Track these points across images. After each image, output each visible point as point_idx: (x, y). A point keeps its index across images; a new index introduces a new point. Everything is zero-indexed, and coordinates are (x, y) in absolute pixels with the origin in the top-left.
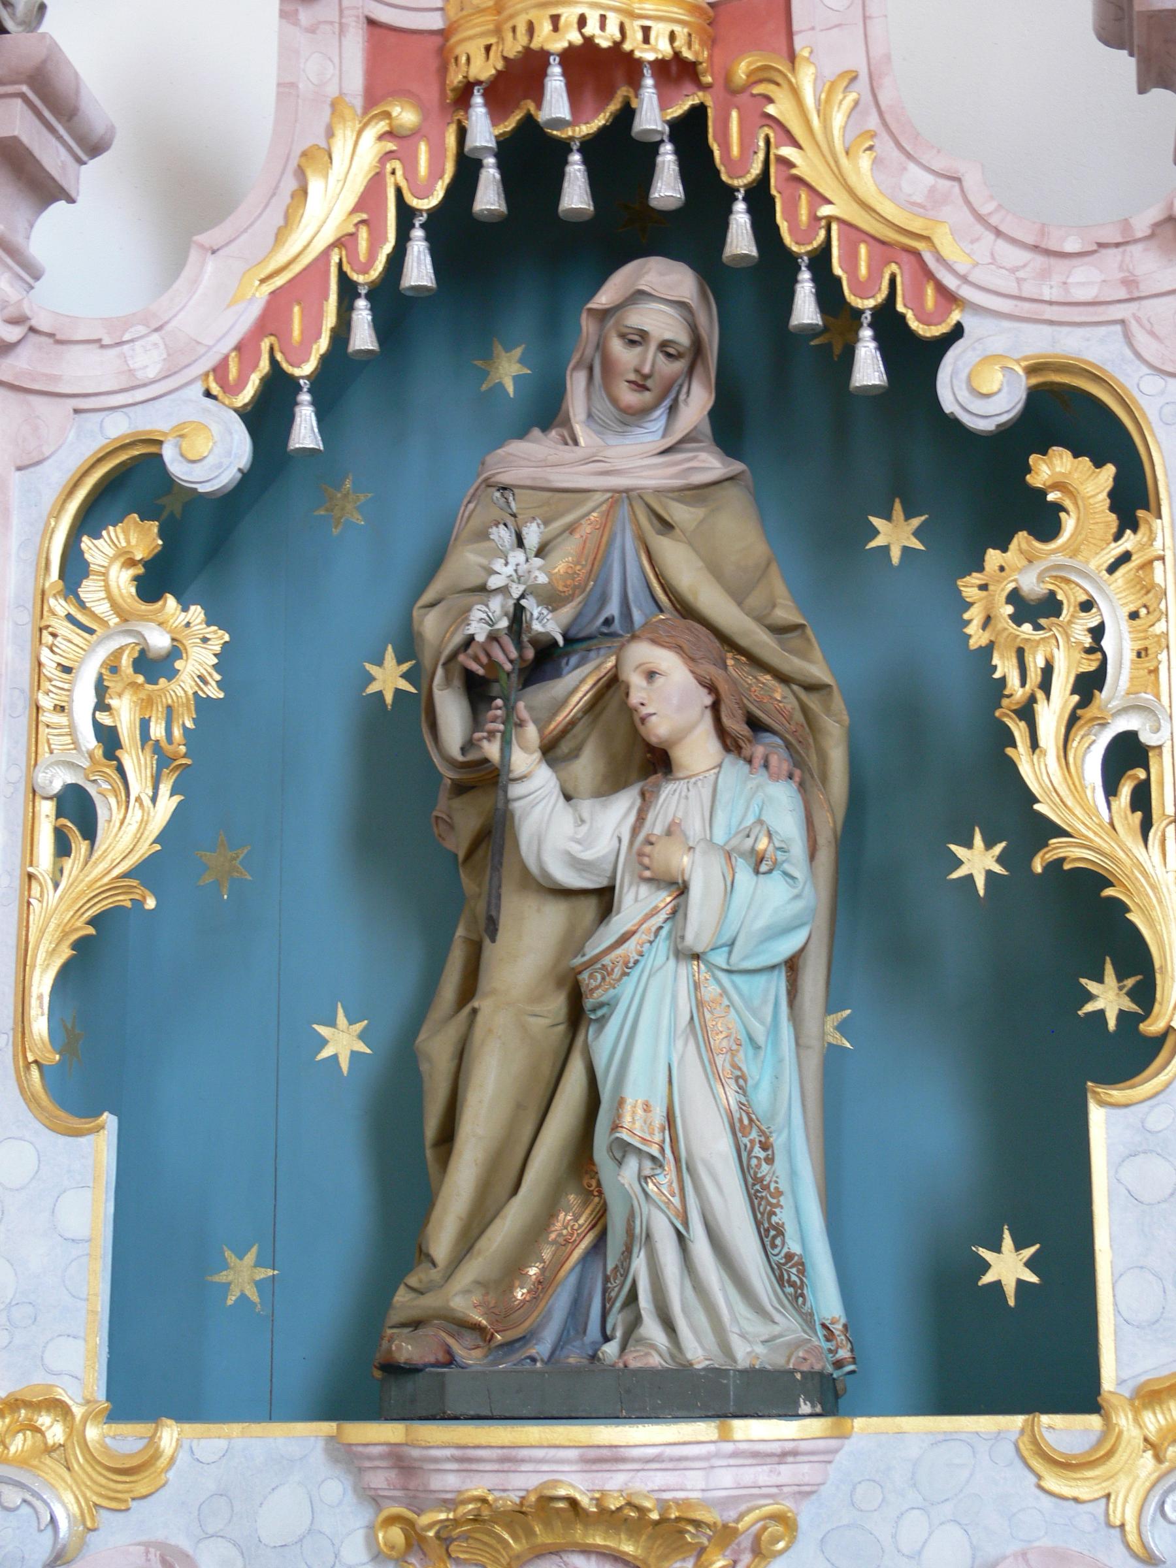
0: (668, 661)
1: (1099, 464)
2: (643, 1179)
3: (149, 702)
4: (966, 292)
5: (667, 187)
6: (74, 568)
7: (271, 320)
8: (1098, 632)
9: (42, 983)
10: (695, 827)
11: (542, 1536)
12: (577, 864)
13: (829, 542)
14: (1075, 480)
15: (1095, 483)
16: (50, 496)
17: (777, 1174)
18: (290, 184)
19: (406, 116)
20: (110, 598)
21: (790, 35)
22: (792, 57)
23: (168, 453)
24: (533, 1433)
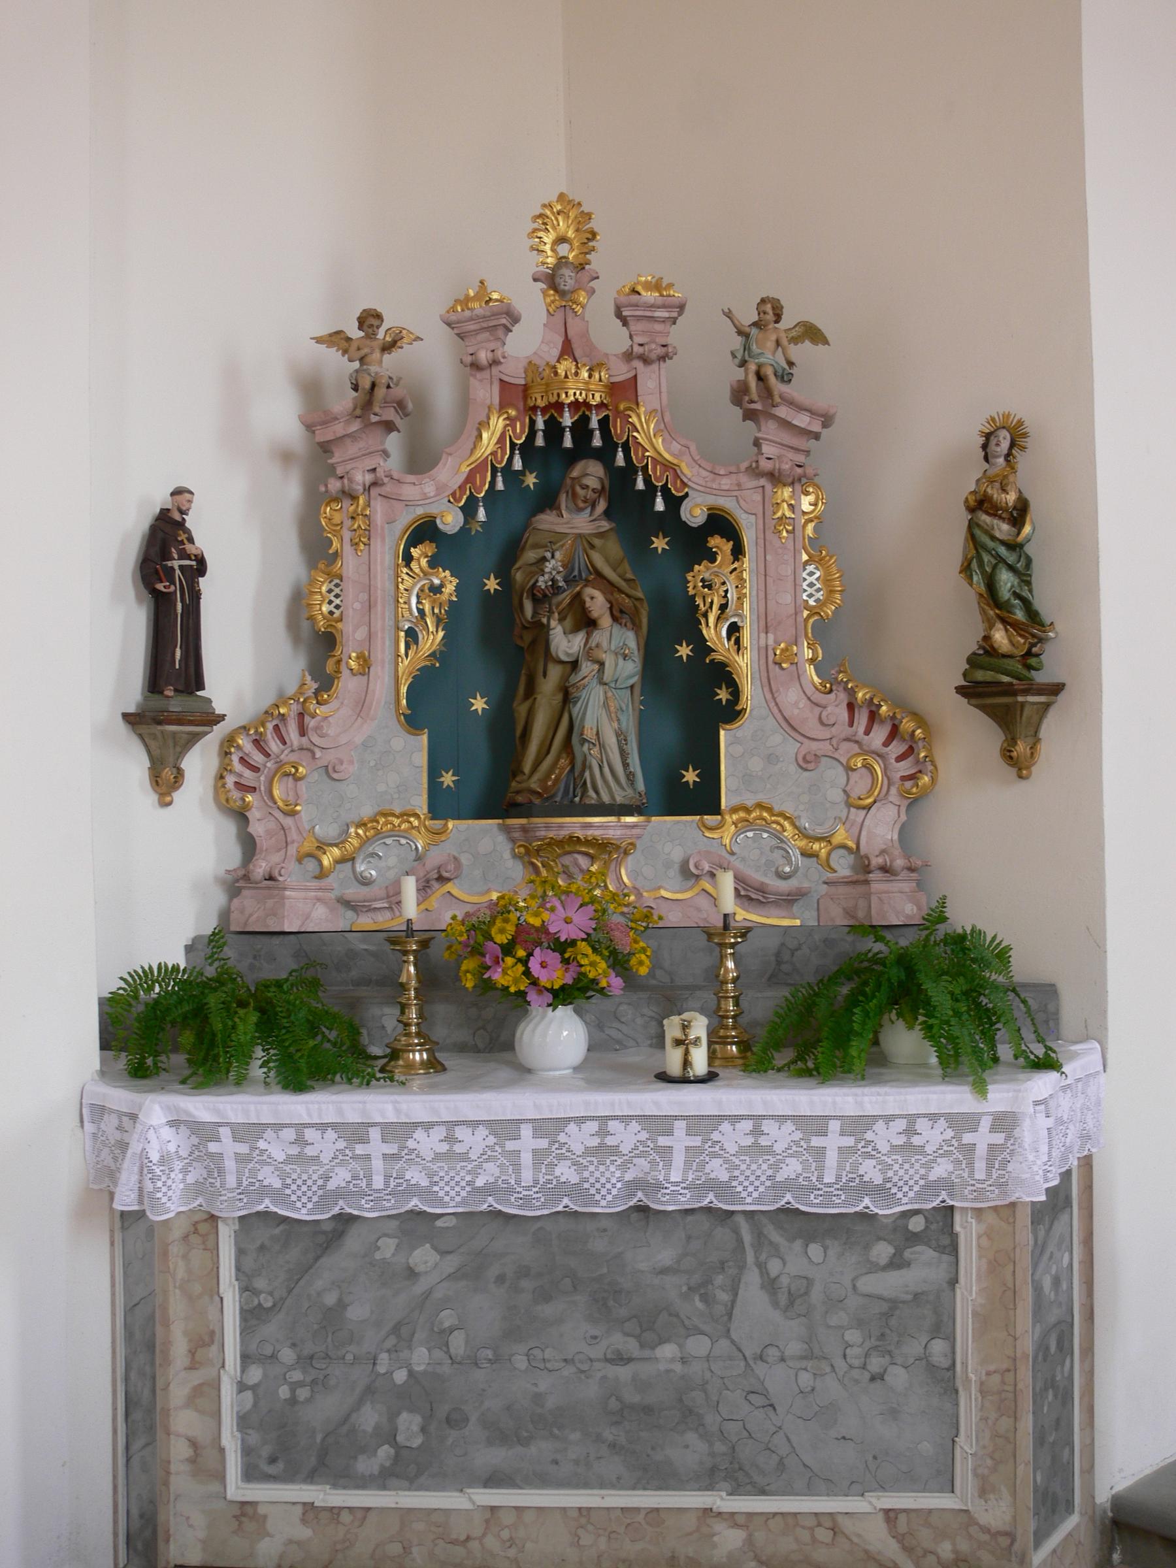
0: (597, 594)
1: (728, 541)
2: (590, 749)
3: (434, 601)
4: (690, 483)
5: (597, 442)
6: (408, 559)
7: (470, 478)
8: (726, 592)
9: (404, 690)
10: (605, 645)
11: (567, 848)
12: (568, 654)
13: (637, 547)
14: (721, 545)
15: (728, 547)
16: (398, 533)
17: (627, 748)
18: (475, 433)
19: (513, 413)
20: (420, 567)
21: (637, 396)
22: (637, 404)
23: (438, 521)
24: (568, 820)
